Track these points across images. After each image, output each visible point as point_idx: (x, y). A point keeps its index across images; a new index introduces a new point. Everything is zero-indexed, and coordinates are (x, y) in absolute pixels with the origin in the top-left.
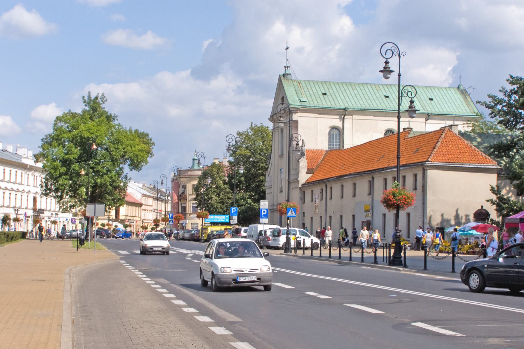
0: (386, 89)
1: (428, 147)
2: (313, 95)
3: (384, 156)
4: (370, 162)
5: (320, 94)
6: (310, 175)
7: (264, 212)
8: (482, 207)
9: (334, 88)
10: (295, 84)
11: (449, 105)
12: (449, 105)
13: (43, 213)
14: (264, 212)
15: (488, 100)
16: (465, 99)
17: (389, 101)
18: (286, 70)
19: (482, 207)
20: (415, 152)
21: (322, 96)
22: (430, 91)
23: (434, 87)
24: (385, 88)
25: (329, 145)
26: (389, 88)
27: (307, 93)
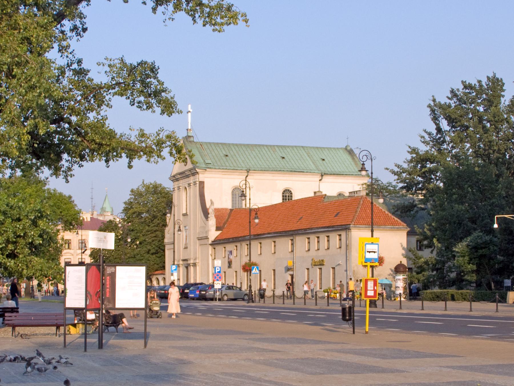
0: (282, 151)
1: (349, 212)
2: (215, 157)
3: (302, 217)
4: (289, 223)
5: (222, 155)
6: (219, 232)
7: (218, 269)
8: (401, 262)
9: (233, 149)
10: (198, 146)
11: (339, 165)
12: (339, 165)
13: (264, 290)
14: (218, 269)
15: (396, 169)
16: (353, 159)
17: (286, 162)
18: (189, 133)
19: (401, 262)
20: (336, 216)
21: (224, 158)
22: (321, 152)
23: (324, 148)
24: (280, 148)
25: (233, 204)
26: (284, 149)
27: (210, 155)
